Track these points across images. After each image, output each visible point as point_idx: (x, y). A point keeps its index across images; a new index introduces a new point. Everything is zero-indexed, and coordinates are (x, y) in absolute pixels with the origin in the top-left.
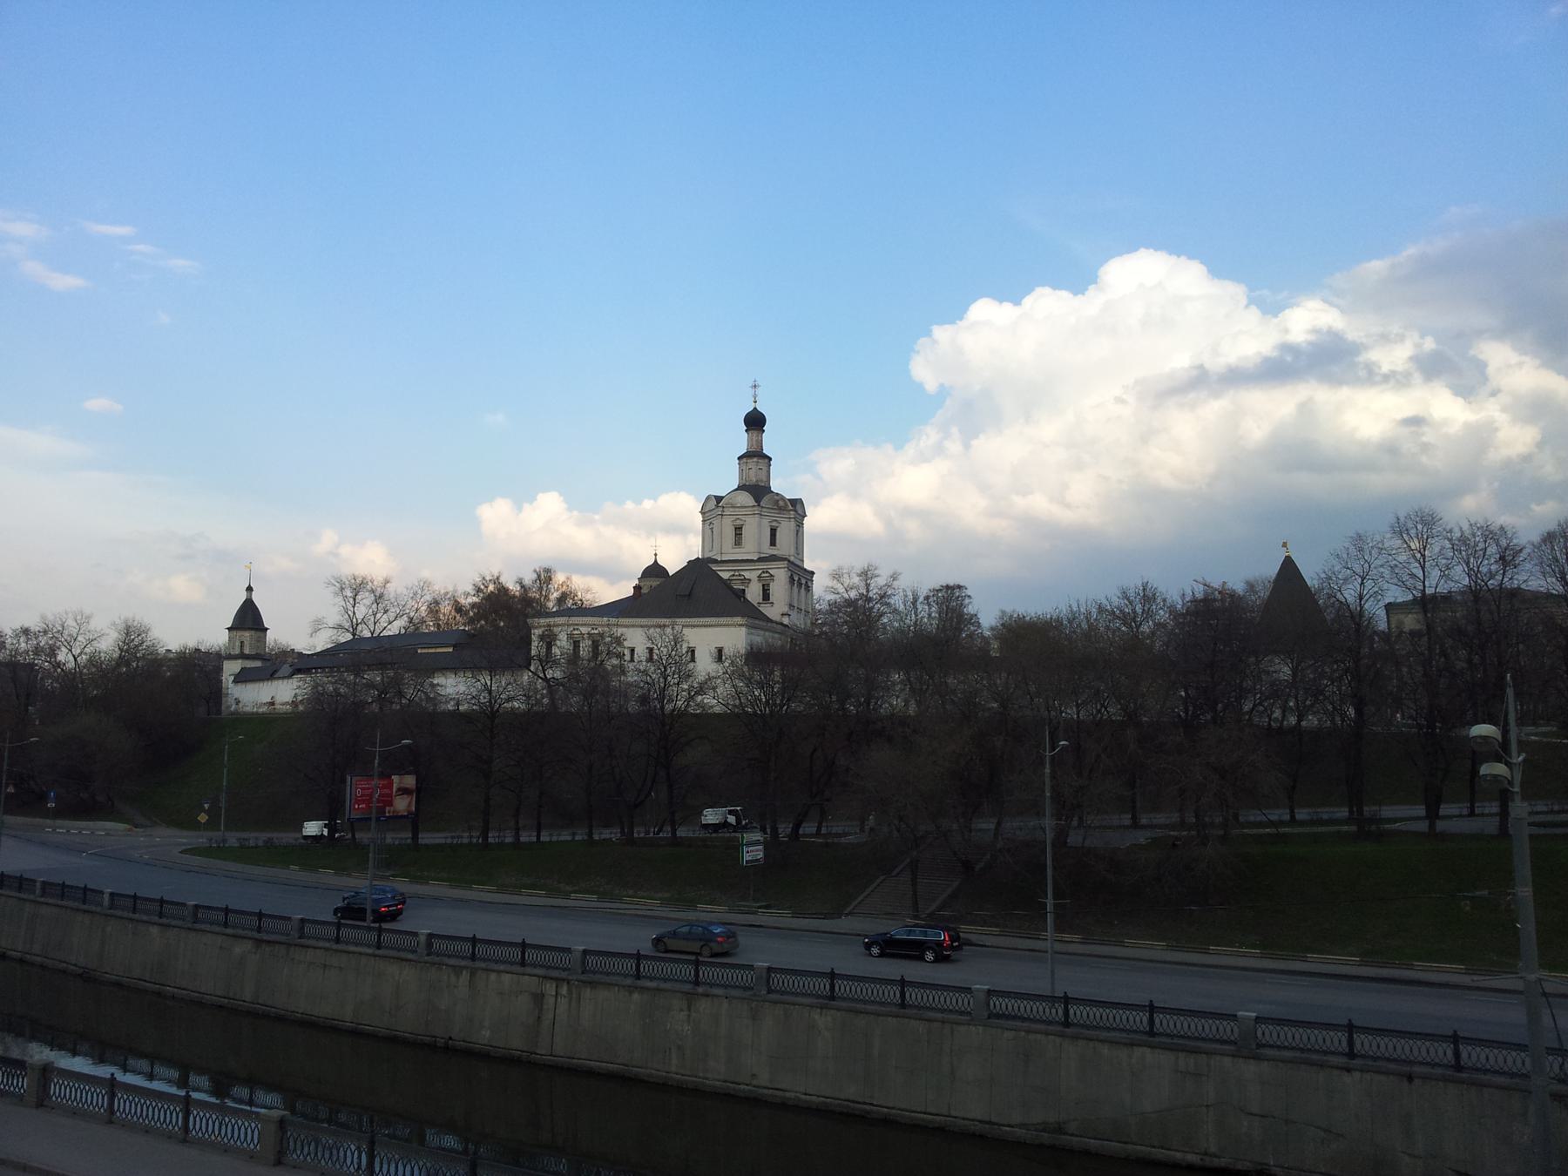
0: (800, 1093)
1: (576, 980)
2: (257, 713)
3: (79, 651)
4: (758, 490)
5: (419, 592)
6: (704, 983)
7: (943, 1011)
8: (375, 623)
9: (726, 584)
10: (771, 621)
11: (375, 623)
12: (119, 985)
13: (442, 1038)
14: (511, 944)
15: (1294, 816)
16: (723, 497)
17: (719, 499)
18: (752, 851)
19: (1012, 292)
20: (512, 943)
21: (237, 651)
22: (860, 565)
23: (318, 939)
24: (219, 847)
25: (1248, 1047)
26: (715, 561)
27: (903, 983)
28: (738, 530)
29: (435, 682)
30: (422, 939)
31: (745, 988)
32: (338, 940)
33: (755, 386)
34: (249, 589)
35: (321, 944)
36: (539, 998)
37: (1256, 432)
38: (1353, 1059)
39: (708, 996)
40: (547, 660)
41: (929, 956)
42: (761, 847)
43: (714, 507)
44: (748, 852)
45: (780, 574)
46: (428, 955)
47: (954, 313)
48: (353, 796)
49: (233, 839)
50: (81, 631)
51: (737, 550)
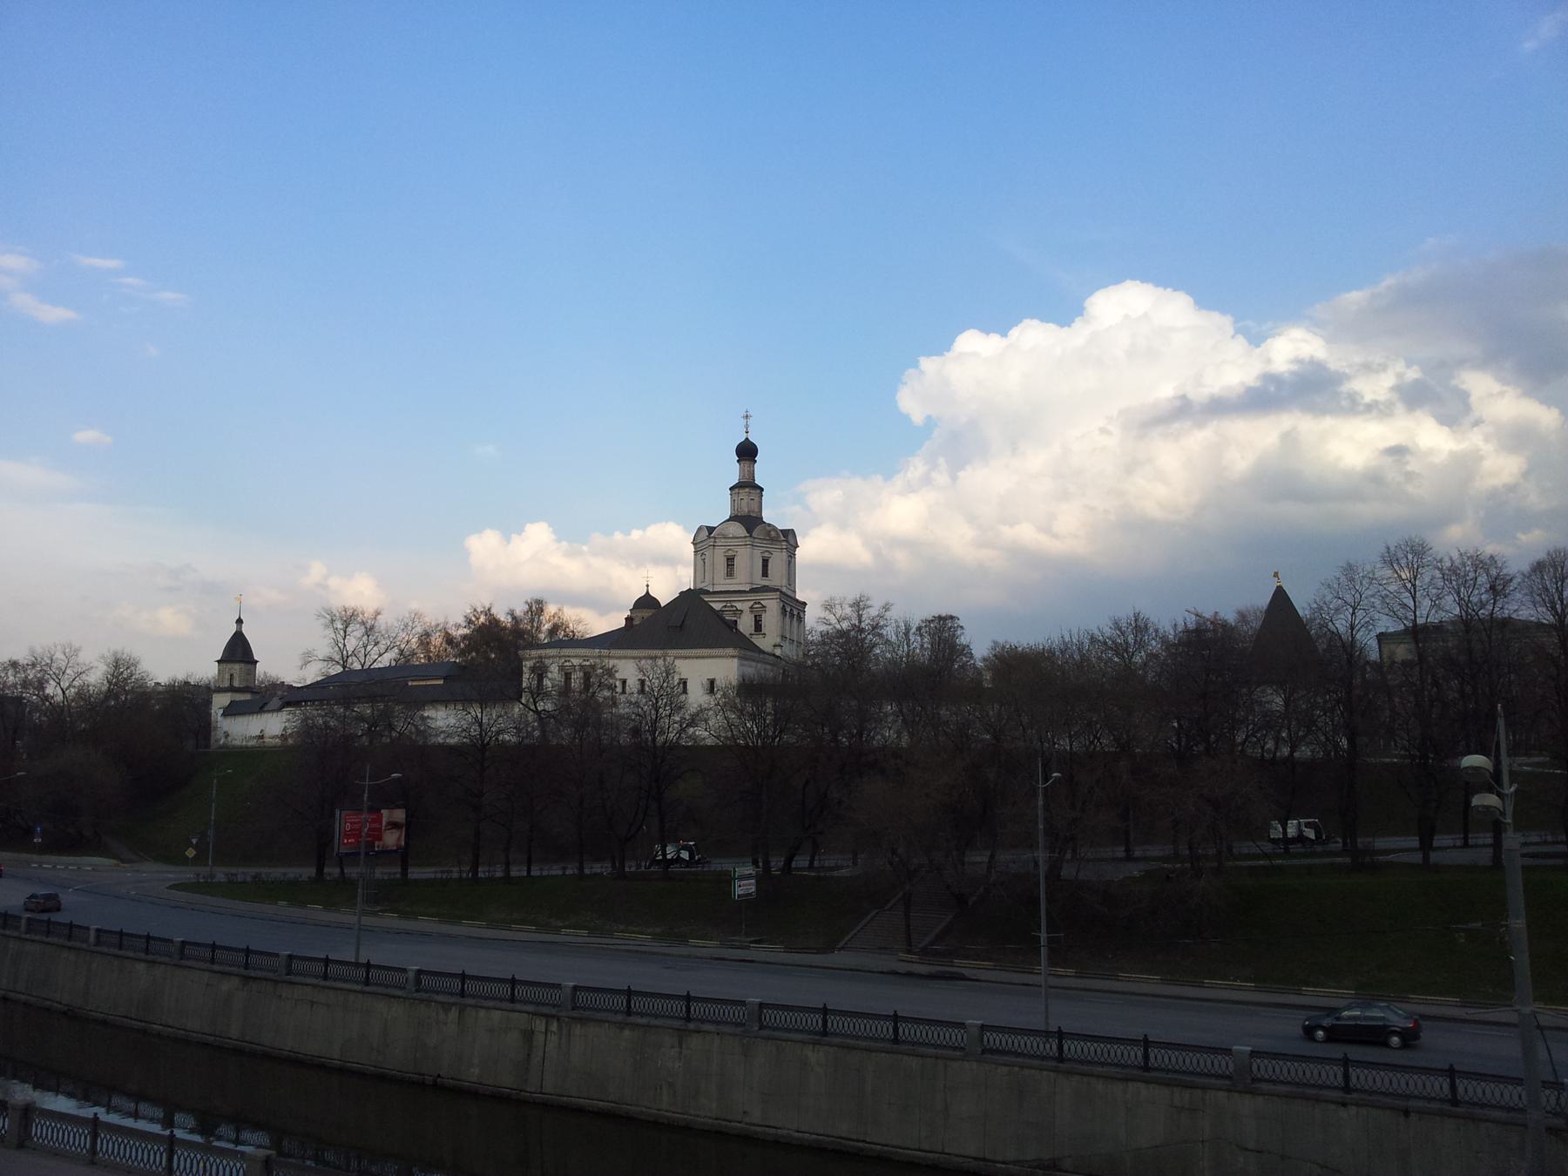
2: (247, 747)
3: (67, 684)
4: (749, 520)
5: (410, 624)
7: (936, 1046)
8: (365, 656)
9: (718, 615)
10: (764, 652)
11: (365, 656)
12: (104, 1023)
17: (711, 530)
18: (744, 885)
21: (227, 684)
26: (707, 592)
28: (730, 561)
29: (426, 715)
30: (411, 975)
31: (737, 1025)
32: (325, 977)
33: (747, 416)
34: (240, 621)
35: (309, 980)
36: (528, 1035)
37: (1240, 462)
40: (538, 692)
42: (753, 881)
43: (706, 539)
44: (740, 886)
45: (772, 605)
46: (417, 991)
48: (342, 831)
49: (220, 874)
50: (70, 665)
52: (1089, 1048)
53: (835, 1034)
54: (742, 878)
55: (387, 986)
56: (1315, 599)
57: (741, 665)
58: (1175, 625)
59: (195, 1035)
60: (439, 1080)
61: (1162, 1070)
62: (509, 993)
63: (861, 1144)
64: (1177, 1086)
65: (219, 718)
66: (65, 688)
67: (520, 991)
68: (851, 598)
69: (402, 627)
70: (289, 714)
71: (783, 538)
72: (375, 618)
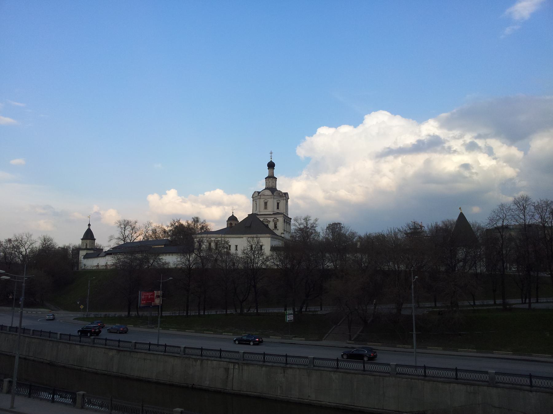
0: (327, 402)
1: (242, 363)
2: (92, 269)
3: (27, 247)
4: (272, 189)
5: (147, 226)
6: (267, 362)
7: (379, 372)
8: (132, 237)
9: (262, 222)
10: (277, 235)
11: (132, 237)
12: (64, 367)
13: (190, 384)
14: (197, 349)
15: (475, 303)
16: (260, 192)
17: (259, 193)
18: (289, 317)
19: (335, 124)
20: (195, 348)
21: (85, 247)
22: (304, 216)
23: (142, 349)
24: (87, 317)
25: (492, 383)
26: (258, 215)
27: (119, 341)
28: (266, 204)
29: (160, 258)
30: (182, 349)
31: (305, 365)
32: (149, 350)
33: (271, 153)
34: (89, 225)
35: (143, 351)
36: (227, 370)
37: (410, 171)
38: (426, 377)
39: (291, 368)
40: (200, 250)
41: (252, 343)
42: (292, 316)
43: (257, 196)
44: (288, 317)
45: (281, 219)
46: (184, 354)
47: (312, 132)
48: (141, 298)
49: (92, 315)
50: (28, 240)
51: (264, 211)
52: (435, 372)
53: (341, 368)
54: (288, 315)
55: (173, 353)
56: (490, 216)
57: (271, 240)
58: (428, 226)
59: (100, 371)
60: (194, 386)
61: (462, 379)
62: (219, 355)
63: (353, 407)
64: (469, 385)
65: (82, 259)
66: (26, 248)
67: (204, 353)
68: (304, 217)
69: (145, 227)
70: (112, 258)
71: (284, 196)
72: (135, 224)
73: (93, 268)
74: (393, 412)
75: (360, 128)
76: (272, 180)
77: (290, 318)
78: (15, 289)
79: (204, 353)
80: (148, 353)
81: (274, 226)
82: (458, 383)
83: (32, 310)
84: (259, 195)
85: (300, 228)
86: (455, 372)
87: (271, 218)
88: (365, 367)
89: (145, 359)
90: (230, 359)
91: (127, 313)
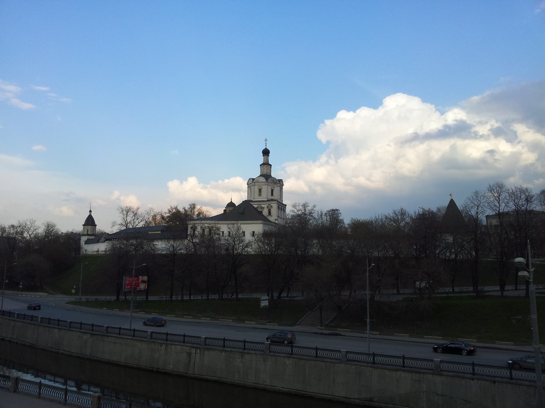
2: (93, 254)
3: (31, 233)
4: (267, 176)
7: (330, 359)
8: (134, 223)
9: (256, 209)
10: (271, 222)
11: (134, 223)
12: (43, 349)
16: (255, 179)
17: (253, 179)
18: (264, 303)
19: (353, 107)
21: (86, 233)
22: (302, 202)
26: (252, 201)
28: (260, 190)
30: (149, 333)
32: (120, 334)
33: (266, 140)
34: (90, 211)
35: (114, 335)
36: (189, 354)
37: (436, 156)
38: (374, 364)
39: (248, 353)
40: (193, 236)
42: (267, 301)
43: (252, 183)
45: (275, 206)
46: (151, 339)
48: (126, 284)
49: (84, 298)
50: (32, 226)
51: (260, 197)
57: (264, 226)
60: (158, 370)
63: (304, 392)
64: (415, 372)
65: (84, 245)
66: (30, 234)
71: (278, 182)
73: (94, 254)
74: (342, 399)
75: (380, 112)
76: (267, 167)
77: (264, 303)
78: (5, 274)
79: (169, 337)
80: (118, 337)
81: (268, 212)
82: (404, 371)
83: (26, 293)
84: (254, 181)
85: (297, 215)
86: (402, 360)
87: (265, 205)
88: (317, 354)
89: (115, 343)
90: (192, 343)
91: (115, 298)
